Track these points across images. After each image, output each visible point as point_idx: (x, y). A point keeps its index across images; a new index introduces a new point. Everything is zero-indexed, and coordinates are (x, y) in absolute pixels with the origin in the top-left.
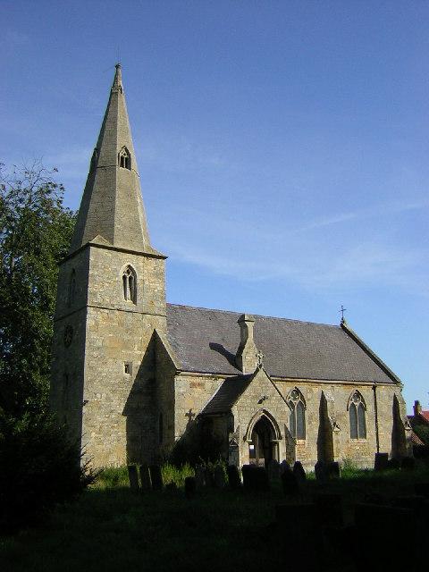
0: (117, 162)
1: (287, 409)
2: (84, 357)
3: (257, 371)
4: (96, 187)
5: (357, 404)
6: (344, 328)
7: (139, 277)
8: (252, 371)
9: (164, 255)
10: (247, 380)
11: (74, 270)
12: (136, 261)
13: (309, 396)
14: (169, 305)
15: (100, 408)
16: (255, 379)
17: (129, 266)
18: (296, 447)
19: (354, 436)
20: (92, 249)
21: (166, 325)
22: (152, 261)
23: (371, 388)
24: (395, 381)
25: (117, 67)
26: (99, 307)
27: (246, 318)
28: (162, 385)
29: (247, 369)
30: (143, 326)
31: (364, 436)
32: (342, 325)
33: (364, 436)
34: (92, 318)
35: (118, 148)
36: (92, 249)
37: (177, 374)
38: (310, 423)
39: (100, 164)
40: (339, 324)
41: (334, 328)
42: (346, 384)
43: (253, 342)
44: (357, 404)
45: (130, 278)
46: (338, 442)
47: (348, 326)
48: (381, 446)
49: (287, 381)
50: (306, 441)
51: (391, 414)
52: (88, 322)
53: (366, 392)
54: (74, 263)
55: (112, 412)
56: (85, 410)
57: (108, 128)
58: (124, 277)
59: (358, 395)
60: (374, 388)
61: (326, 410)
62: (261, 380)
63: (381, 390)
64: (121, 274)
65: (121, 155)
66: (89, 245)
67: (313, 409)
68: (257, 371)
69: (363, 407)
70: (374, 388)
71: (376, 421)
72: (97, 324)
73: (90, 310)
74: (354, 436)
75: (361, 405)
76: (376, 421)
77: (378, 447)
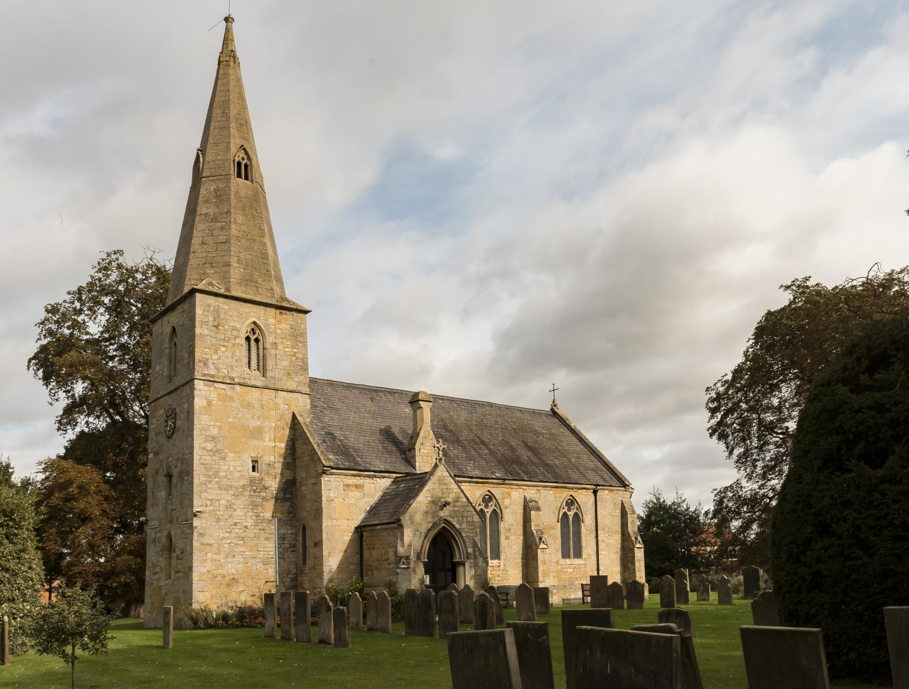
0: (233, 171)
1: (476, 518)
2: (192, 453)
3: (436, 466)
4: (202, 209)
5: (571, 514)
6: (554, 413)
7: (270, 340)
8: (428, 469)
9: (307, 308)
10: (422, 480)
11: (174, 329)
12: (268, 319)
13: (507, 502)
14: (313, 381)
15: (218, 520)
16: (433, 479)
17: (254, 323)
18: (490, 569)
19: (565, 555)
20: (198, 296)
21: (308, 407)
22: (288, 316)
23: (590, 493)
24: (623, 484)
25: (227, 19)
26: (211, 381)
27: (420, 397)
28: (303, 488)
29: (422, 464)
30: (277, 407)
31: (578, 554)
32: (552, 410)
33: (578, 554)
34: (202, 394)
35: (233, 149)
36: (198, 296)
37: (324, 472)
38: (507, 538)
39: (206, 173)
40: (548, 408)
41: (547, 415)
42: (556, 487)
43: (429, 428)
44: (571, 514)
45: (246, 166)
46: (544, 562)
47: (560, 411)
48: (601, 568)
49: (477, 483)
50: (502, 562)
51: (619, 529)
52: (196, 400)
53: (585, 498)
54: (173, 319)
55: (236, 524)
56: (196, 522)
57: (217, 112)
58: (248, 339)
59: (571, 502)
60: (595, 492)
61: (530, 521)
62: (441, 481)
63: (603, 494)
64: (244, 335)
65: (237, 159)
66: (193, 291)
67: (512, 520)
68: (436, 466)
69: (577, 519)
70: (595, 492)
71: (597, 537)
72: (210, 403)
73: (198, 384)
74: (565, 555)
75: (576, 514)
76: (597, 537)
77: (598, 570)
